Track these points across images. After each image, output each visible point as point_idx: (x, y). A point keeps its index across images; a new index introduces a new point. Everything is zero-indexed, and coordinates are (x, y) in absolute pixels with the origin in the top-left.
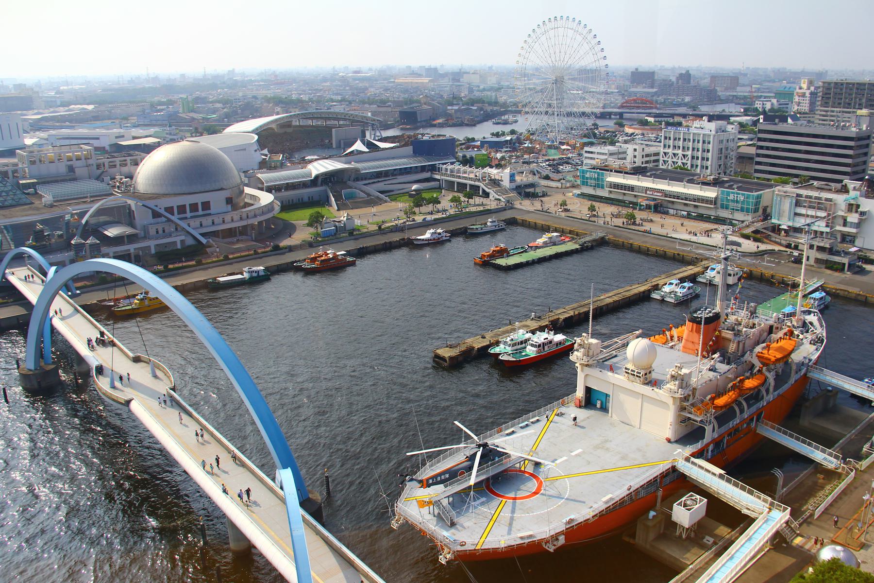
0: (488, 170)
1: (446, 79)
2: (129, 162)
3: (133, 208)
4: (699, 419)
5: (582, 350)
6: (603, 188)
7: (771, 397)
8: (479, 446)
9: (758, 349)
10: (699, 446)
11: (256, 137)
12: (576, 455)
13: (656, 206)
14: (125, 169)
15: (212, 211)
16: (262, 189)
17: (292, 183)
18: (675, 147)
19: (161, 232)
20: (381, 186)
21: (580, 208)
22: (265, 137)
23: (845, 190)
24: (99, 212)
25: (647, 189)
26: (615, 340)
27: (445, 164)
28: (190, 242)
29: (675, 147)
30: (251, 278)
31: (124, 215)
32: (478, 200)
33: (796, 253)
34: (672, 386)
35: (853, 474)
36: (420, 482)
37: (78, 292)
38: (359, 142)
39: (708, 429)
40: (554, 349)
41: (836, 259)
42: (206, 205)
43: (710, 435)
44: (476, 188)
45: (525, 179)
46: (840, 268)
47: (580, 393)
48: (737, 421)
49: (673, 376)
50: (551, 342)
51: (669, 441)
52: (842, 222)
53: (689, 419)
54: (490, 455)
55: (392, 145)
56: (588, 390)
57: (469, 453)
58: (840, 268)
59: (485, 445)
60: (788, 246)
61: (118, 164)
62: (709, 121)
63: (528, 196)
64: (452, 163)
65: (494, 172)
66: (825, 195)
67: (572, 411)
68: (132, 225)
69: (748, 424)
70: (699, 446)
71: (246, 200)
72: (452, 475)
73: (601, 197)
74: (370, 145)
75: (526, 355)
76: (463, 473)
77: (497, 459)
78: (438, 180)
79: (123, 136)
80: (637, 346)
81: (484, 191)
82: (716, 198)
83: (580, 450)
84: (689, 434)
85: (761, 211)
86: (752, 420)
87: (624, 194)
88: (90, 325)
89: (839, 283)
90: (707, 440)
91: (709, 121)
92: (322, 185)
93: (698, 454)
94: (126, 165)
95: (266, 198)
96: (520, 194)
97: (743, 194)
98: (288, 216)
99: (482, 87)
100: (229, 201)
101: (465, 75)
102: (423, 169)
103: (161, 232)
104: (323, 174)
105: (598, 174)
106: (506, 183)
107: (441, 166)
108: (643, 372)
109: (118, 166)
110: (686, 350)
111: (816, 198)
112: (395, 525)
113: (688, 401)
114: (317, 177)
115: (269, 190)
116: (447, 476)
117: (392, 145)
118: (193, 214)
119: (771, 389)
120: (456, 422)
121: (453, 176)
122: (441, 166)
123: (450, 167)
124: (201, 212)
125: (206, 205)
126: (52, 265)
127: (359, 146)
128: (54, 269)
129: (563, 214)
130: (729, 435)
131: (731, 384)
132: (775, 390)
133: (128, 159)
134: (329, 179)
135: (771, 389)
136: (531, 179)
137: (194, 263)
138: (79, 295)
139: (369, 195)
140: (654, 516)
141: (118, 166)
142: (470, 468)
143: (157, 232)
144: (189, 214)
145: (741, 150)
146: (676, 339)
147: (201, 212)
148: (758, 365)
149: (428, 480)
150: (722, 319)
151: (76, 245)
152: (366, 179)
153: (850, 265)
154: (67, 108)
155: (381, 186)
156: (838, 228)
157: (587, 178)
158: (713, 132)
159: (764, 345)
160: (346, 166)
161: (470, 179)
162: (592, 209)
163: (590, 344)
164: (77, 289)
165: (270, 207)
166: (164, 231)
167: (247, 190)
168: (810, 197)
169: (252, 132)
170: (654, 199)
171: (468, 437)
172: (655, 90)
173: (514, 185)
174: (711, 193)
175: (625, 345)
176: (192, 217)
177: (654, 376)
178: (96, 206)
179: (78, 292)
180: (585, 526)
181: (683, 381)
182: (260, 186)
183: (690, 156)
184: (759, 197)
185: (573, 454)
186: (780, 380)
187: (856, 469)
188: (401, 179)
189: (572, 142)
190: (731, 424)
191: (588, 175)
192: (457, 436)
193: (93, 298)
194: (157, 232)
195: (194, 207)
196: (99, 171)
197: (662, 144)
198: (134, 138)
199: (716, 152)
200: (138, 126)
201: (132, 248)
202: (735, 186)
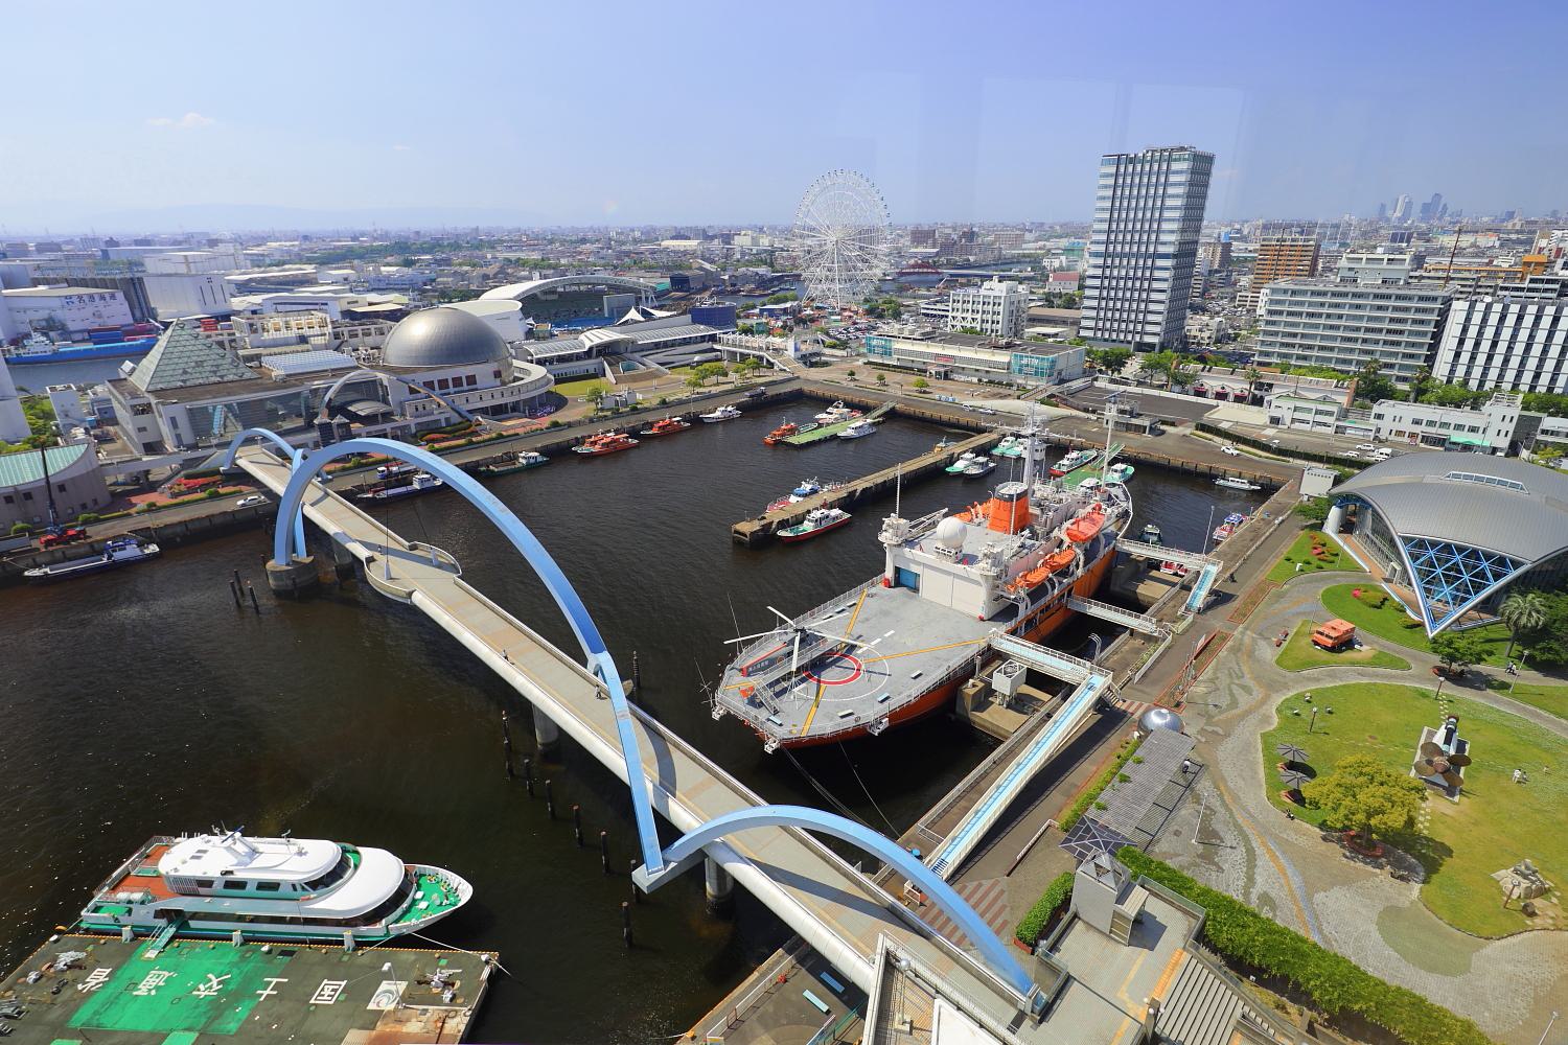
0: (771, 339)
1: (716, 241)
2: (373, 331)
3: (385, 383)
4: (1013, 597)
5: (891, 531)
6: (890, 355)
8: (797, 631)
9: (1067, 524)
10: (1012, 624)
11: (520, 305)
13: (946, 373)
14: (369, 340)
15: (478, 386)
16: (532, 362)
17: (564, 355)
18: (963, 311)
19: (421, 408)
20: (661, 357)
21: (869, 378)
22: (531, 305)
24: (346, 387)
25: (938, 356)
26: (922, 519)
28: (456, 418)
29: (963, 311)
30: (528, 464)
31: (370, 390)
32: (763, 371)
34: (984, 565)
35: (1170, 637)
36: (741, 670)
37: (330, 477)
38: (633, 309)
39: (1022, 607)
40: (831, 523)
41: (1135, 421)
42: (471, 380)
43: (1022, 613)
45: (810, 349)
46: (1140, 429)
47: (889, 573)
48: (1048, 597)
49: (985, 555)
50: (827, 517)
51: (982, 619)
53: (1002, 596)
54: (807, 639)
55: (669, 314)
56: (897, 570)
57: (787, 638)
58: (1140, 429)
59: (803, 631)
61: (360, 333)
62: (1000, 281)
63: (812, 365)
64: (733, 333)
65: (777, 341)
67: (880, 588)
68: (385, 401)
69: (1059, 600)
70: (1012, 624)
71: (516, 374)
72: (771, 662)
73: (888, 365)
74: (645, 314)
76: (781, 660)
77: (814, 644)
78: (718, 350)
79: (357, 302)
80: (948, 525)
81: (768, 360)
82: (1009, 363)
83: (892, 632)
84: (1004, 612)
85: (1055, 374)
86: (1063, 596)
87: (913, 361)
88: (352, 513)
90: (1019, 618)
91: (1000, 281)
92: (597, 357)
93: (1013, 632)
94: (370, 335)
95: (539, 372)
96: (805, 363)
97: (1037, 358)
98: (564, 389)
99: (754, 251)
100: (498, 374)
101: (736, 237)
102: (703, 339)
103: (421, 408)
104: (598, 346)
105: (886, 340)
106: (791, 353)
107: (722, 336)
108: (953, 551)
109: (360, 335)
110: (993, 526)
112: (716, 716)
113: (1001, 579)
114: (591, 349)
115: (540, 362)
116: (767, 663)
117: (669, 314)
118: (456, 389)
119: (1081, 564)
120: (770, 608)
121: (735, 346)
122: (722, 336)
123: (731, 337)
125: (471, 380)
126: (295, 447)
127: (633, 314)
128: (300, 452)
129: (852, 384)
130: (1042, 612)
131: (1042, 561)
133: (372, 327)
134: (606, 351)
135: (1081, 564)
136: (816, 348)
138: (331, 480)
140: (950, 718)
141: (360, 335)
142: (790, 653)
143: (417, 409)
144: (452, 389)
145: (1031, 312)
146: (980, 515)
147: (465, 387)
148: (1067, 540)
149: (748, 668)
150: (1029, 495)
151: (321, 426)
152: (643, 350)
153: (1151, 428)
154: (280, 268)
158: (1004, 294)
159: (1072, 521)
160: (623, 336)
161: (754, 348)
162: (881, 378)
163: (898, 525)
164: (329, 473)
165: (543, 381)
166: (424, 408)
167: (516, 363)
169: (515, 298)
170: (944, 366)
171: (783, 622)
172: (935, 250)
173: (799, 354)
174: (1003, 357)
175: (934, 524)
176: (455, 393)
177: (967, 550)
178: (341, 381)
179: (330, 477)
180: (906, 709)
181: (995, 559)
182: (529, 358)
183: (979, 320)
184: (1053, 362)
186: (1090, 555)
187: (1174, 632)
188: (680, 349)
189: (854, 308)
190: (1043, 602)
191: (874, 343)
192: (770, 623)
193: (348, 483)
194: (417, 409)
195: (457, 382)
196: (338, 341)
197: (950, 309)
198: (370, 304)
199: (1007, 313)
200: (373, 290)
201: (388, 427)
202: (1029, 349)
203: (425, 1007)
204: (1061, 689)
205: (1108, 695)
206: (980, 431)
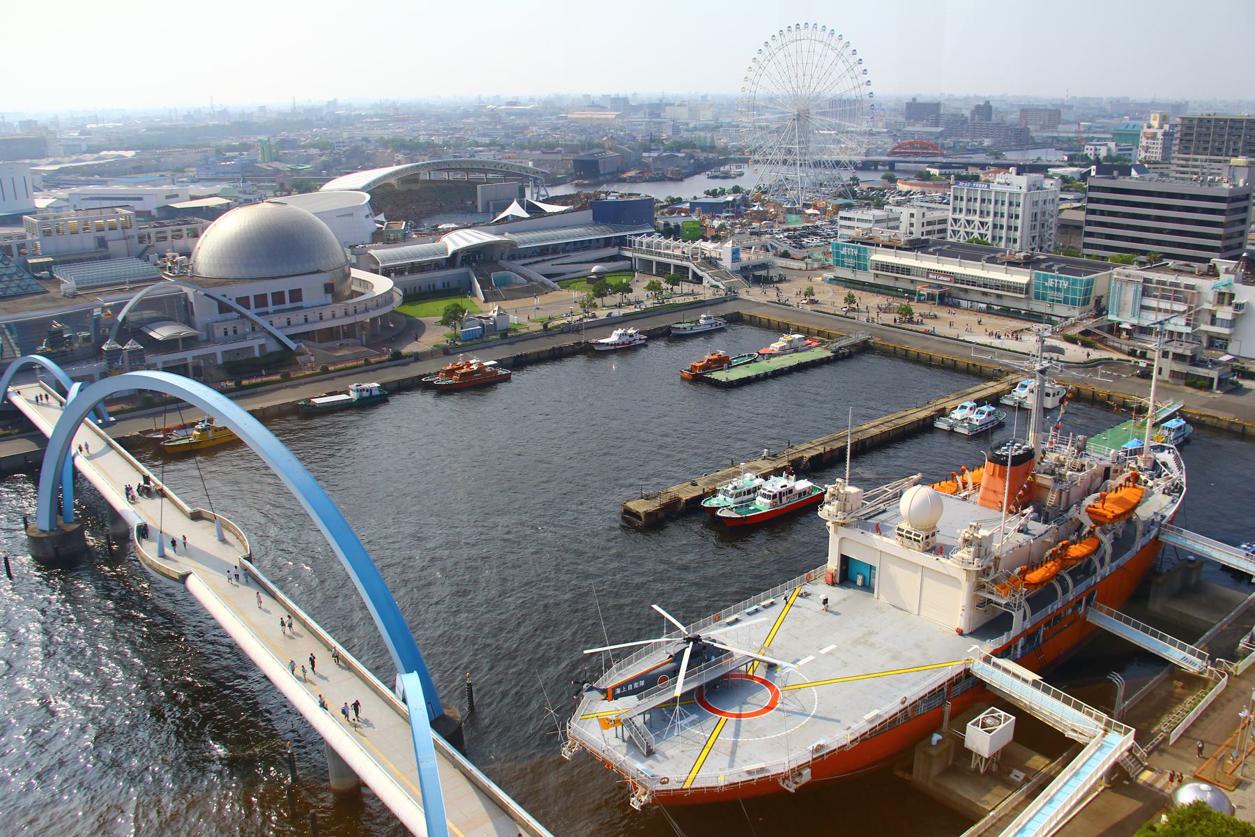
0: (700, 244)
1: (641, 114)
2: (185, 232)
3: (191, 298)
4: (1004, 602)
5: (836, 502)
6: (865, 269)
7: (1106, 570)
8: (688, 640)
9: (1089, 501)
10: (1003, 640)
11: (368, 197)
12: (828, 654)
13: (942, 296)
14: (179, 243)
15: (305, 303)
16: (376, 272)
17: (420, 263)
18: (969, 211)
19: (231, 333)
20: (548, 267)
21: (832, 299)
22: (381, 197)
23: (1213, 273)
24: (143, 304)
25: (929, 271)
26: (884, 488)
27: (639, 235)
28: (273, 347)
29: (969, 211)
30: (361, 399)
31: (179, 309)
32: (686, 287)
33: (1143, 364)
34: (965, 554)
36: (604, 691)
37: (112, 419)
38: (515, 204)
39: (1017, 616)
41: (1201, 371)
42: (296, 295)
43: (1019, 624)
44: (683, 270)
45: (753, 258)
46: (1205, 384)
47: (833, 564)
48: (1058, 604)
49: (966, 540)
50: (791, 491)
51: (961, 633)
52: (1208, 319)
53: (990, 601)
54: (704, 653)
55: (563, 208)
56: (845, 560)
57: (673, 650)
58: (1205, 384)
59: (696, 639)
60: (1132, 353)
61: (169, 235)
62: (1018, 174)
63: (758, 281)
64: (649, 235)
65: (709, 247)
66: (1184, 280)
68: (189, 322)
69: (1075, 609)
70: (1003, 640)
71: (353, 288)
72: (649, 682)
73: (863, 283)
74: (531, 208)
75: (756, 510)
76: (664, 679)
77: (713, 659)
78: (629, 259)
79: (177, 196)
80: (914, 496)
81: (695, 274)
82: (1028, 285)
83: (833, 646)
84: (989, 623)
85: (1092, 302)
86: (1080, 602)
87: (897, 279)
88: (130, 467)
89: (1205, 406)
90: (1015, 632)
91: (1018, 174)
92: (462, 266)
93: (1003, 652)
94: (181, 237)
95: (382, 285)
96: (746, 278)
97: (1066, 279)
98: (414, 311)
99: (691, 125)
100: (329, 288)
101: (668, 108)
102: (607, 242)
103: (231, 333)
104: (463, 250)
105: (859, 249)
106: (727, 263)
107: (633, 238)
108: (923, 535)
109: (169, 238)
110: (984, 502)
111: (1172, 284)
112: (566, 754)
113: (988, 575)
114: (455, 254)
115: (386, 273)
116: (642, 683)
117: (563, 208)
118: (277, 307)
119: (1107, 558)
120: (655, 607)
121: (651, 253)
122: (633, 238)
123: (646, 240)
124: (288, 305)
125: (296, 295)
126: (74, 380)
127: (515, 209)
128: (77, 386)
129: (809, 308)
130: (1047, 624)
131: (1050, 551)
132: (1112, 560)
133: (184, 228)
134: (472, 257)
135: (1107, 558)
136: (762, 257)
137: (278, 377)
138: (113, 423)
139: (529, 280)
140: (939, 741)
141: (169, 238)
142: (675, 672)
143: (226, 333)
144: (271, 308)
145: (1064, 216)
146: (970, 486)
147: (288, 305)
148: (1088, 523)
149: (614, 689)
150: (1037, 458)
151: (110, 352)
152: (525, 257)
153: (1220, 380)
154: (96, 156)
155: (548, 267)
156: (1204, 327)
157: (843, 256)
158: (1024, 190)
159: (1097, 495)
160: (497, 238)
161: (675, 257)
162: (850, 300)
163: (847, 494)
164: (111, 414)
165: (387, 297)
166: (235, 332)
167: (355, 273)
168: (1164, 283)
169: (362, 189)
170: (940, 286)
171: (672, 628)
172: (940, 129)
173: (738, 266)
174: (1021, 277)
175: (898, 496)
176: (275, 312)
178: (138, 296)
179: (112, 419)
180: (840, 755)
181: (980, 547)
182: (374, 267)
183: (990, 224)
184: (1090, 283)
185: (823, 652)
186: (1120, 545)
188: (576, 256)
189: (822, 203)
190: (1050, 609)
191: (844, 252)
192: (656, 627)
193: (133, 428)
194: (226, 333)
195: (278, 297)
196: (143, 246)
197: (950, 207)
198: (193, 198)
199: (1028, 218)
200: (199, 181)
201: (189, 356)
202: (1055, 267)
203: (1128, 556)
204: (1062, 748)
205: (1130, 766)
206: (995, 376)
